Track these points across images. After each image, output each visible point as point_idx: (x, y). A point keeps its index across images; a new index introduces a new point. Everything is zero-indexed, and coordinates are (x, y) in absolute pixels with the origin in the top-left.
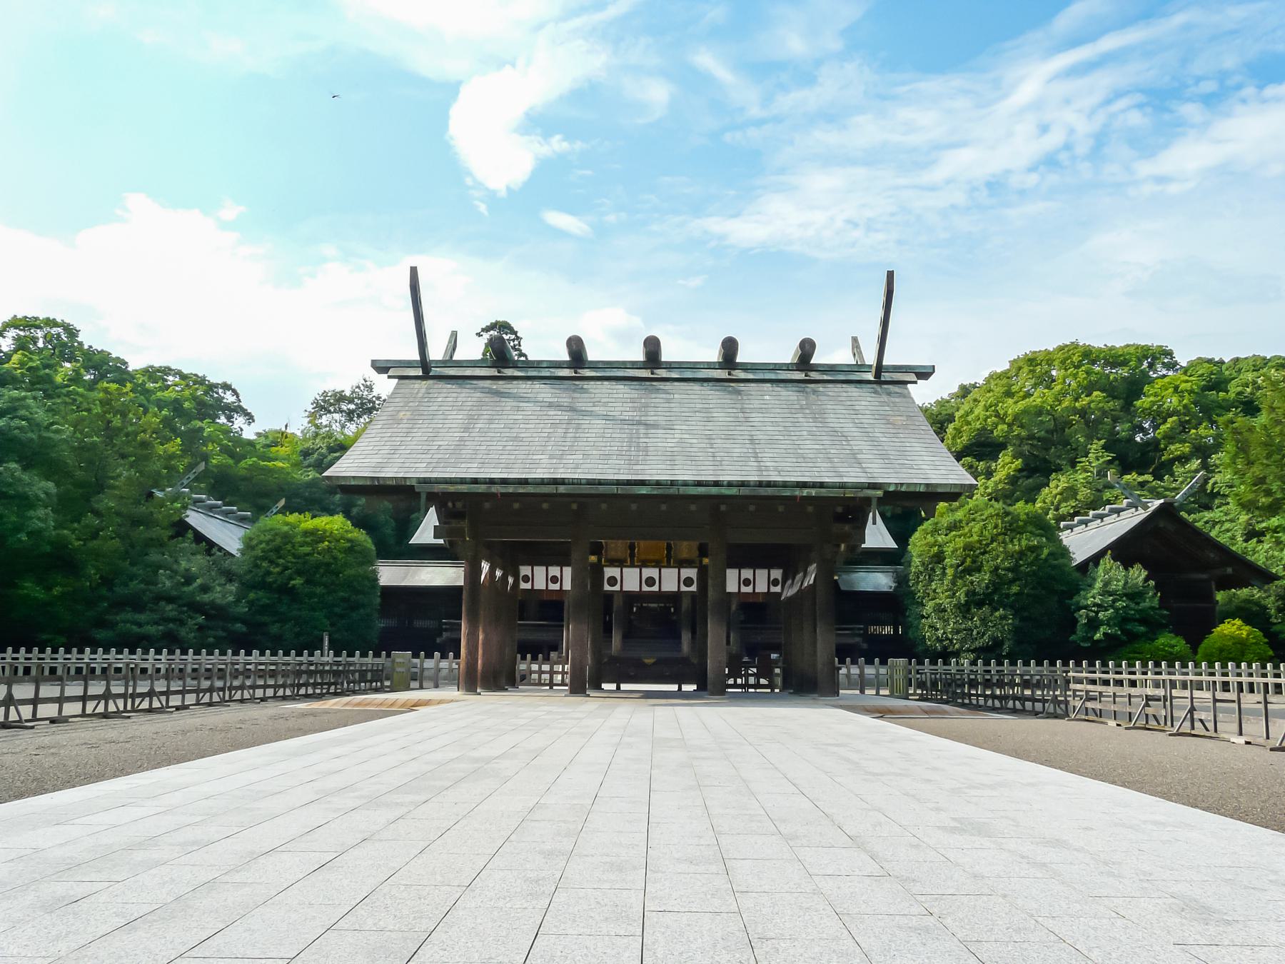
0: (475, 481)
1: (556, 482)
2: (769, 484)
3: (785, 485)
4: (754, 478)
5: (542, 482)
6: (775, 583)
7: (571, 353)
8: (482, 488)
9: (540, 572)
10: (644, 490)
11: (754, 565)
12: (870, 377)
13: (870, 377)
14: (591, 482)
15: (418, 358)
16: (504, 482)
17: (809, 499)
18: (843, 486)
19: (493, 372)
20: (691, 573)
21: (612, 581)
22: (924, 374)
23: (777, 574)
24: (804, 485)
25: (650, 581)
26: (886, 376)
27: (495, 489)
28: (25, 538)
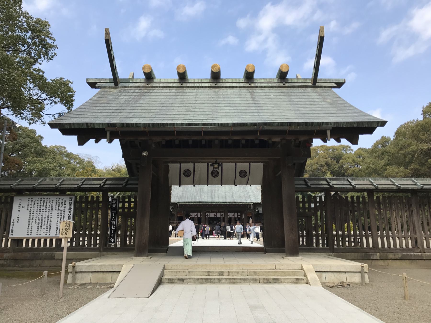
0: (187, 202)
1: (200, 202)
2: (234, 202)
3: (237, 202)
4: (232, 201)
5: (198, 202)
6: (239, 215)
7: (179, 74)
8: (188, 203)
9: (193, 214)
10: (214, 203)
11: (235, 212)
12: (310, 84)
13: (310, 84)
14: (206, 202)
15: (112, 77)
16: (192, 202)
17: (242, 205)
18: (246, 202)
19: (213, 85)
20: (223, 214)
21: (207, 215)
22: (383, 124)
23: (239, 214)
24: (240, 202)
25: (215, 215)
26: (318, 84)
27: (190, 203)
28: (344, 197)
